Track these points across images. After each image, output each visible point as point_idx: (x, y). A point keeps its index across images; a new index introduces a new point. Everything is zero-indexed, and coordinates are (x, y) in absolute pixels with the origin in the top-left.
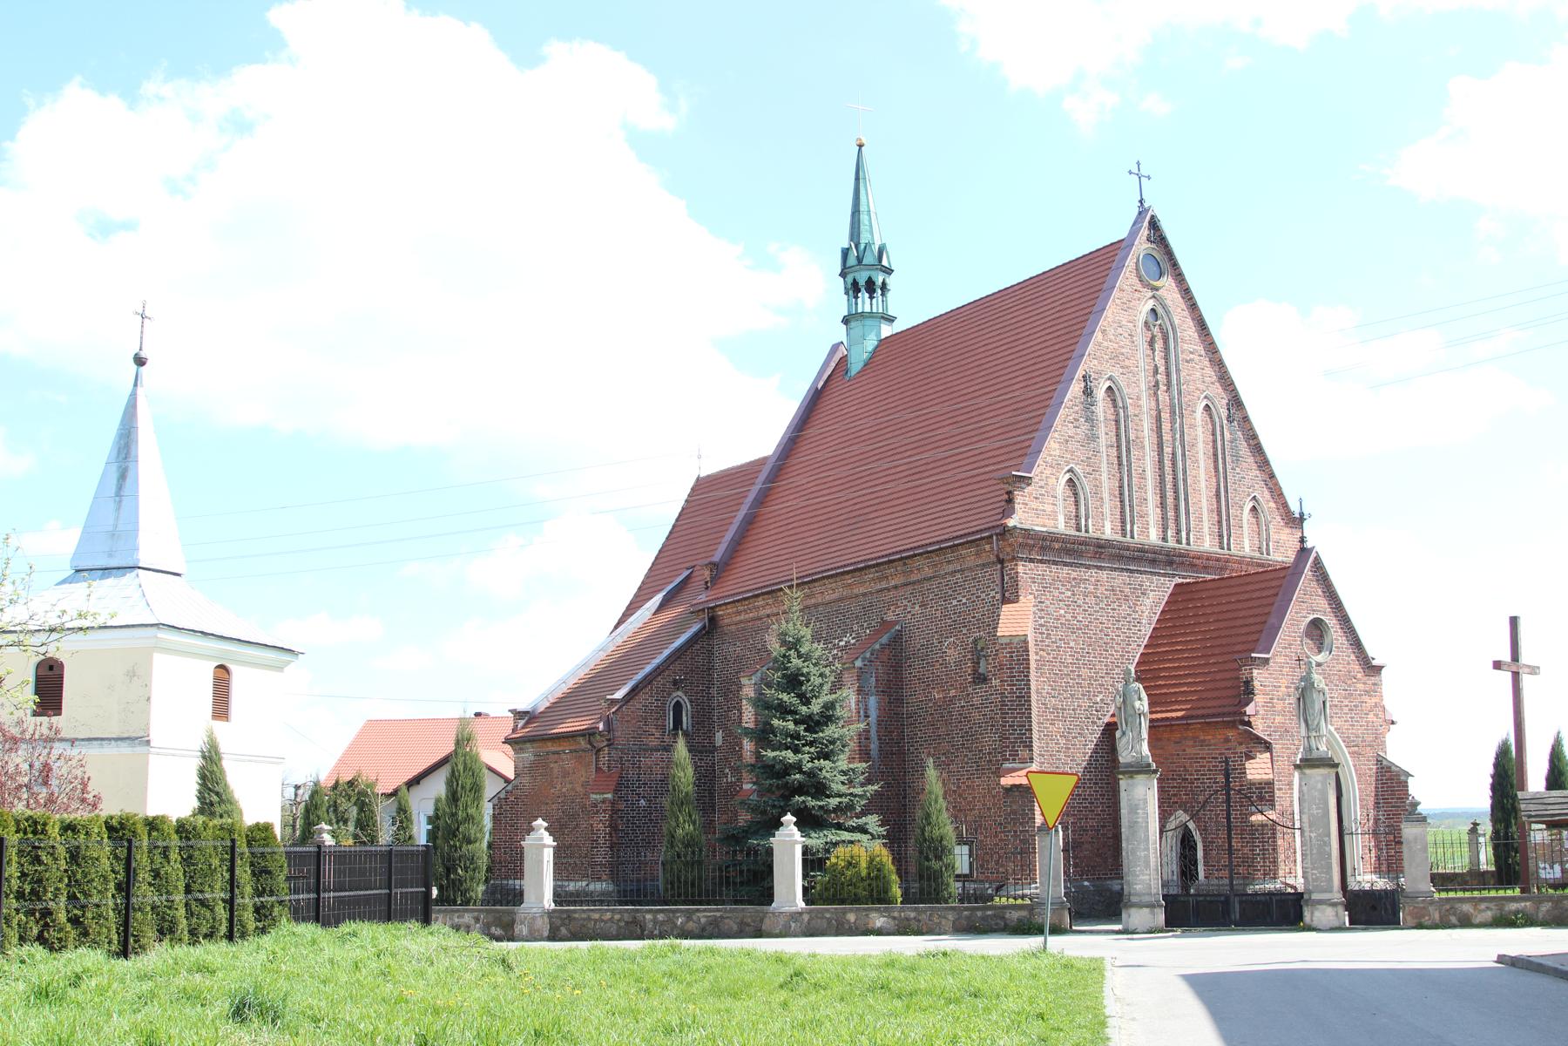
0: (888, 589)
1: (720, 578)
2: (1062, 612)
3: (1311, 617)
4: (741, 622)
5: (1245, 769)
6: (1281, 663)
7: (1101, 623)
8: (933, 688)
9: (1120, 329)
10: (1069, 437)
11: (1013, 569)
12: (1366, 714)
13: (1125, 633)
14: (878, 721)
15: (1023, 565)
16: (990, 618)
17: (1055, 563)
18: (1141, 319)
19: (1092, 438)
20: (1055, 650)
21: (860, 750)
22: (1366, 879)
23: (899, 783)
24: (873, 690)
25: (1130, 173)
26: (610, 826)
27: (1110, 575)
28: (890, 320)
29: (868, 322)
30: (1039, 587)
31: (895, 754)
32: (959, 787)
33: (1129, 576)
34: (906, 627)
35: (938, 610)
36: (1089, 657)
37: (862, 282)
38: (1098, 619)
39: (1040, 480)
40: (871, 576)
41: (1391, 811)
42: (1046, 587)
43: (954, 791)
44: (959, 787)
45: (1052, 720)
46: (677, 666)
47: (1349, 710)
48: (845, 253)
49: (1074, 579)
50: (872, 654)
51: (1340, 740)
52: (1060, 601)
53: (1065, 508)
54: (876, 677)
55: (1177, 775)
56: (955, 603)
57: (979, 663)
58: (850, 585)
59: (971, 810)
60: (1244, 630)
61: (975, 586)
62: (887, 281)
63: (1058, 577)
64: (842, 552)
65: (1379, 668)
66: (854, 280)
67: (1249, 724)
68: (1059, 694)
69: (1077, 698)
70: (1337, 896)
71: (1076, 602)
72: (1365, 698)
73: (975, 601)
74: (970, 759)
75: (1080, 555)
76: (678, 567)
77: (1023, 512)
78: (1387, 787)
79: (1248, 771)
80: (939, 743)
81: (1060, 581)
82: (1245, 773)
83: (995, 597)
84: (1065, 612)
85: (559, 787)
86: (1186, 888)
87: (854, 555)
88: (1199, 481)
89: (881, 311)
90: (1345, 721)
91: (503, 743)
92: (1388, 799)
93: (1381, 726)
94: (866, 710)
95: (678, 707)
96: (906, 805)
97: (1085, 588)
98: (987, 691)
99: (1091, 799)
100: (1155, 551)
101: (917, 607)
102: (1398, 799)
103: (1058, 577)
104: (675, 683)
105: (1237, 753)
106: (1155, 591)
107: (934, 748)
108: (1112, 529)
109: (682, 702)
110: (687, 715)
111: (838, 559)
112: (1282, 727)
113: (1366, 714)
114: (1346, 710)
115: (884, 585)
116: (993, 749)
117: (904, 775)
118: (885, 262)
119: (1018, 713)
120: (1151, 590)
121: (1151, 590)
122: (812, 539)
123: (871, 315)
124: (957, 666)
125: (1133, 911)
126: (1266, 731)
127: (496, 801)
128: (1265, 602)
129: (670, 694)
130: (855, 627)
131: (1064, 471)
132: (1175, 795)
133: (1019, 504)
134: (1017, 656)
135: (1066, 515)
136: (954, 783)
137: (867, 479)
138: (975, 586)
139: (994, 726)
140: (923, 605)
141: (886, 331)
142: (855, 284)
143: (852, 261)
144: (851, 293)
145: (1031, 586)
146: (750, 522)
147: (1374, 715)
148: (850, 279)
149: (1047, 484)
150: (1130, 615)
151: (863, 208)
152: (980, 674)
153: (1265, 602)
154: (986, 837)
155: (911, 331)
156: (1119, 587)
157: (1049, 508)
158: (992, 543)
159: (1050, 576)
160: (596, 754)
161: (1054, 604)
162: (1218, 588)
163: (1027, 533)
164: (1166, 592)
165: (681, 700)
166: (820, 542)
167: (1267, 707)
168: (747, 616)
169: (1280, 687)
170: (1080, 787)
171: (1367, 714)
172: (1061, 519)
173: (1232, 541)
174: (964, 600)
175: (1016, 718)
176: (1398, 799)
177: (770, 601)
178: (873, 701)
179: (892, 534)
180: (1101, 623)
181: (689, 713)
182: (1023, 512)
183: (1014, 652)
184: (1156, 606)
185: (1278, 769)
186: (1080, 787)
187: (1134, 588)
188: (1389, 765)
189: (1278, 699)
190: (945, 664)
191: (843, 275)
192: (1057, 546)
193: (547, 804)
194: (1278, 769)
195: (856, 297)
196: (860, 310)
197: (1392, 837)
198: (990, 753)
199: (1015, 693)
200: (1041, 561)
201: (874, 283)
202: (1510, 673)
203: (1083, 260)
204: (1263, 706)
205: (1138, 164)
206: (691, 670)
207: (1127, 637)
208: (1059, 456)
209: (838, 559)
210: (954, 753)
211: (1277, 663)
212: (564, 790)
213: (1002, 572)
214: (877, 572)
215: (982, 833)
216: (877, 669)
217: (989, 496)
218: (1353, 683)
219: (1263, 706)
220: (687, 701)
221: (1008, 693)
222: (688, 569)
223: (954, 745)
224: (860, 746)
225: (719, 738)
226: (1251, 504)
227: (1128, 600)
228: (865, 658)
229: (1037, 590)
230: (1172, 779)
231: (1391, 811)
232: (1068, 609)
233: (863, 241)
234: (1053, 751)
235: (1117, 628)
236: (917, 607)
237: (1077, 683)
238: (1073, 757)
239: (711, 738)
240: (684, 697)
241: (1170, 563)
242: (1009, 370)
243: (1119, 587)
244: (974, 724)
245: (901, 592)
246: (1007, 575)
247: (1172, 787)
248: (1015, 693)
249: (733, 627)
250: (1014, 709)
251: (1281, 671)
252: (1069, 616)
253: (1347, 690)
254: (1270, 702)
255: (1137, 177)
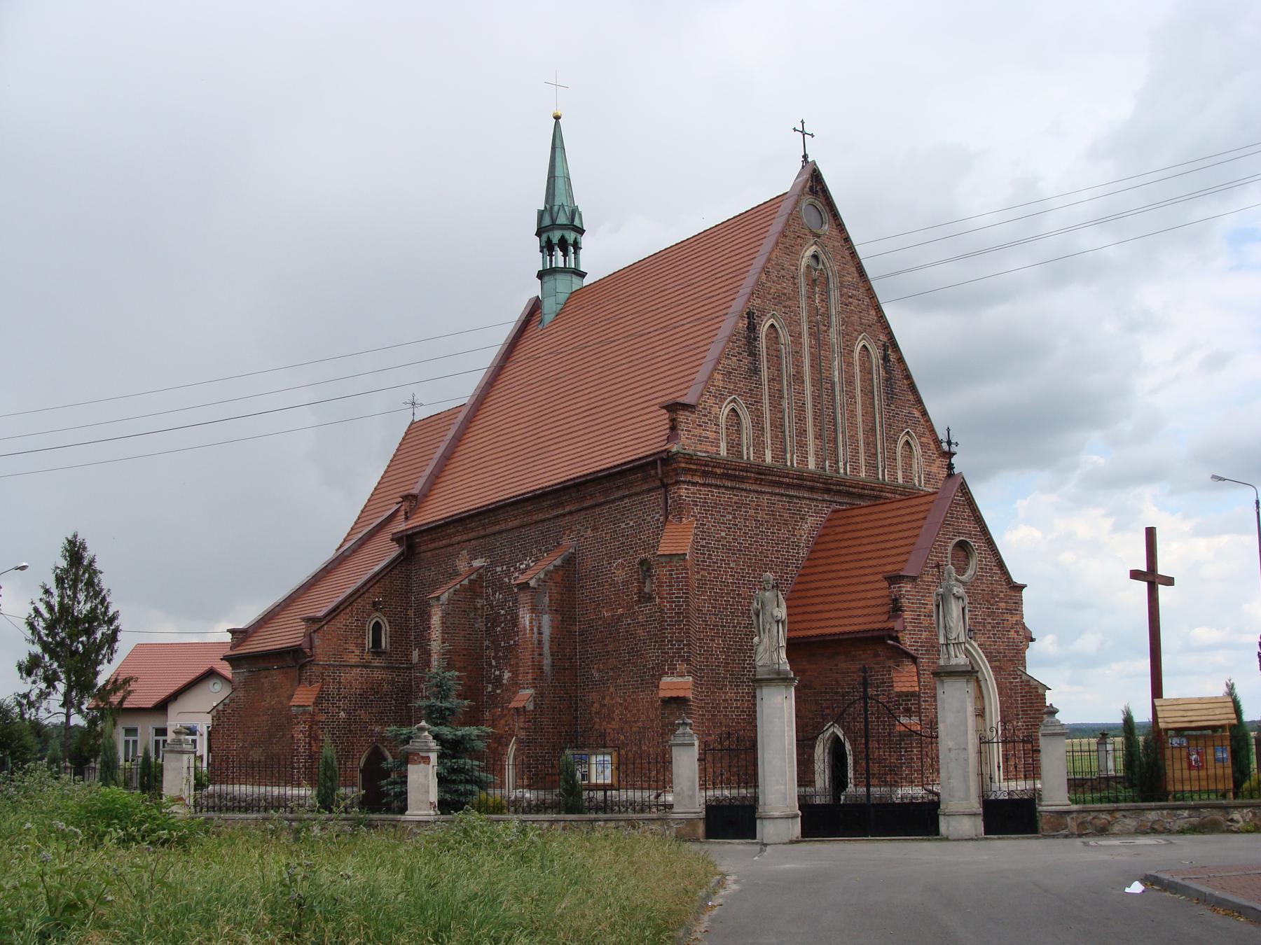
0: (564, 515)
1: (419, 508)
2: (723, 534)
3: (957, 539)
4: (435, 549)
5: (892, 682)
6: (928, 582)
7: (761, 546)
8: (603, 607)
9: (782, 272)
10: (733, 369)
11: (676, 493)
12: (1007, 631)
13: (784, 555)
14: (551, 638)
15: (686, 489)
16: (654, 539)
17: (717, 486)
18: (803, 263)
19: (755, 371)
20: (716, 570)
21: (532, 665)
22: (1006, 787)
23: (570, 697)
24: (547, 608)
25: (795, 130)
26: (310, 735)
27: (770, 500)
28: (582, 275)
29: (560, 277)
30: (701, 510)
31: (567, 669)
32: (625, 700)
33: (788, 502)
34: (579, 550)
35: (607, 533)
36: (749, 577)
37: (555, 240)
38: (758, 542)
39: (703, 408)
40: (548, 503)
41: (1030, 722)
42: (709, 510)
43: (621, 704)
44: (625, 700)
45: (712, 636)
46: (377, 589)
47: (992, 627)
48: (541, 215)
49: (736, 503)
50: (546, 575)
51: (982, 655)
52: (722, 523)
53: (728, 436)
54: (550, 596)
55: (830, 688)
56: (623, 526)
57: (644, 583)
58: (530, 511)
59: (635, 722)
60: (894, 552)
61: (641, 510)
62: (578, 240)
63: (720, 501)
64: (524, 481)
65: (1022, 587)
66: (549, 238)
67: (896, 639)
68: (719, 611)
69: (737, 616)
70: (976, 806)
71: (737, 525)
72: (1008, 617)
73: (641, 524)
74: (635, 674)
75: (742, 479)
76: (390, 502)
77: (687, 438)
78: (1027, 700)
79: (895, 684)
80: (607, 659)
81: (722, 505)
82: (892, 686)
83: (659, 520)
84: (727, 535)
85: (268, 701)
86: (837, 798)
87: (534, 483)
88: (856, 415)
89: (573, 266)
90: (988, 638)
91: (222, 659)
92: (1027, 711)
93: (1021, 642)
94: (539, 628)
95: (377, 627)
96: (577, 717)
97: (745, 512)
98: (651, 609)
99: (749, 712)
100: (813, 478)
101: (589, 531)
102: (1035, 710)
103: (720, 501)
104: (375, 604)
105: (885, 667)
106: (813, 516)
107: (604, 663)
108: (772, 457)
109: (382, 623)
110: (386, 634)
111: (519, 488)
112: (929, 642)
113: (1007, 631)
114: (988, 627)
115: (560, 512)
116: (656, 664)
117: (576, 690)
118: (577, 222)
119: (676, 629)
120: (809, 516)
121: (809, 516)
122: (499, 471)
123: (565, 270)
124: (625, 585)
125: (766, 823)
126: (914, 646)
127: (214, 712)
128: (914, 525)
129: (369, 615)
130: (534, 551)
131: (728, 400)
132: (828, 708)
133: (683, 430)
134: (676, 574)
135: (728, 443)
136: (620, 697)
137: (551, 415)
138: (641, 510)
139: (657, 642)
140: (595, 529)
141: (577, 284)
142: (549, 241)
143: (547, 221)
144: (545, 250)
145: (693, 509)
146: (447, 458)
147: (1015, 632)
148: (544, 237)
149: (709, 413)
150: (790, 538)
151: (558, 172)
152: (645, 593)
153: (914, 525)
154: (648, 747)
155: (598, 284)
156: (779, 512)
157: (712, 435)
158: (657, 468)
159: (712, 500)
160: (299, 669)
161: (716, 526)
162: (871, 514)
163: (690, 458)
164: (824, 517)
165: (380, 621)
166: (506, 473)
167: (915, 623)
168: (440, 543)
169: (927, 604)
170: (739, 700)
171: (1009, 631)
172: (723, 445)
173: (886, 472)
174: (631, 523)
175: (675, 633)
176: (1035, 710)
177: (460, 529)
178: (546, 619)
179: (568, 463)
180: (761, 546)
181: (388, 633)
182: (687, 438)
183: (673, 570)
184: (814, 531)
185: (924, 682)
186: (739, 700)
187: (793, 513)
188: (1028, 678)
189: (925, 616)
190: (613, 584)
191: (539, 234)
192: (718, 471)
193: (259, 715)
194: (924, 682)
195: (551, 255)
196: (554, 266)
197: (1030, 746)
198: (653, 668)
199: (674, 609)
200: (704, 485)
201: (566, 241)
202: (1146, 583)
203: (751, 212)
204: (911, 622)
205: (803, 122)
206: (390, 593)
207: (786, 559)
208: (723, 387)
209: (519, 488)
210: (620, 668)
211: (924, 581)
212: (273, 703)
213: (666, 496)
214: (554, 499)
215: (645, 744)
216: (551, 589)
217: (656, 425)
218: (997, 602)
219: (911, 622)
220: (386, 621)
221: (668, 610)
222: (397, 503)
223: (621, 661)
224: (533, 661)
225: (415, 655)
226: (905, 439)
227: (787, 524)
228: (540, 579)
229: (699, 513)
230: (825, 693)
231: (1030, 722)
232: (729, 531)
233: (557, 202)
234: (712, 666)
235: (776, 551)
236: (589, 531)
237: (737, 602)
238: (732, 671)
239: (408, 655)
240: (383, 617)
241: (828, 491)
242: (666, 298)
243: (779, 512)
244: (640, 640)
245: (576, 517)
246: (671, 498)
247: (825, 700)
248: (674, 609)
249: (429, 553)
250: (672, 625)
251: (928, 589)
252: (730, 538)
253: (989, 608)
254: (916, 619)
255: (801, 135)
